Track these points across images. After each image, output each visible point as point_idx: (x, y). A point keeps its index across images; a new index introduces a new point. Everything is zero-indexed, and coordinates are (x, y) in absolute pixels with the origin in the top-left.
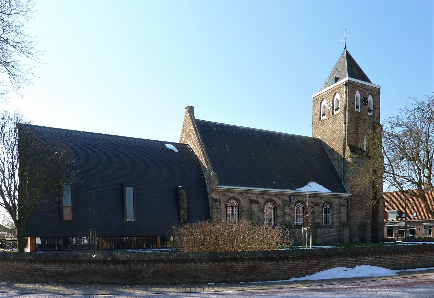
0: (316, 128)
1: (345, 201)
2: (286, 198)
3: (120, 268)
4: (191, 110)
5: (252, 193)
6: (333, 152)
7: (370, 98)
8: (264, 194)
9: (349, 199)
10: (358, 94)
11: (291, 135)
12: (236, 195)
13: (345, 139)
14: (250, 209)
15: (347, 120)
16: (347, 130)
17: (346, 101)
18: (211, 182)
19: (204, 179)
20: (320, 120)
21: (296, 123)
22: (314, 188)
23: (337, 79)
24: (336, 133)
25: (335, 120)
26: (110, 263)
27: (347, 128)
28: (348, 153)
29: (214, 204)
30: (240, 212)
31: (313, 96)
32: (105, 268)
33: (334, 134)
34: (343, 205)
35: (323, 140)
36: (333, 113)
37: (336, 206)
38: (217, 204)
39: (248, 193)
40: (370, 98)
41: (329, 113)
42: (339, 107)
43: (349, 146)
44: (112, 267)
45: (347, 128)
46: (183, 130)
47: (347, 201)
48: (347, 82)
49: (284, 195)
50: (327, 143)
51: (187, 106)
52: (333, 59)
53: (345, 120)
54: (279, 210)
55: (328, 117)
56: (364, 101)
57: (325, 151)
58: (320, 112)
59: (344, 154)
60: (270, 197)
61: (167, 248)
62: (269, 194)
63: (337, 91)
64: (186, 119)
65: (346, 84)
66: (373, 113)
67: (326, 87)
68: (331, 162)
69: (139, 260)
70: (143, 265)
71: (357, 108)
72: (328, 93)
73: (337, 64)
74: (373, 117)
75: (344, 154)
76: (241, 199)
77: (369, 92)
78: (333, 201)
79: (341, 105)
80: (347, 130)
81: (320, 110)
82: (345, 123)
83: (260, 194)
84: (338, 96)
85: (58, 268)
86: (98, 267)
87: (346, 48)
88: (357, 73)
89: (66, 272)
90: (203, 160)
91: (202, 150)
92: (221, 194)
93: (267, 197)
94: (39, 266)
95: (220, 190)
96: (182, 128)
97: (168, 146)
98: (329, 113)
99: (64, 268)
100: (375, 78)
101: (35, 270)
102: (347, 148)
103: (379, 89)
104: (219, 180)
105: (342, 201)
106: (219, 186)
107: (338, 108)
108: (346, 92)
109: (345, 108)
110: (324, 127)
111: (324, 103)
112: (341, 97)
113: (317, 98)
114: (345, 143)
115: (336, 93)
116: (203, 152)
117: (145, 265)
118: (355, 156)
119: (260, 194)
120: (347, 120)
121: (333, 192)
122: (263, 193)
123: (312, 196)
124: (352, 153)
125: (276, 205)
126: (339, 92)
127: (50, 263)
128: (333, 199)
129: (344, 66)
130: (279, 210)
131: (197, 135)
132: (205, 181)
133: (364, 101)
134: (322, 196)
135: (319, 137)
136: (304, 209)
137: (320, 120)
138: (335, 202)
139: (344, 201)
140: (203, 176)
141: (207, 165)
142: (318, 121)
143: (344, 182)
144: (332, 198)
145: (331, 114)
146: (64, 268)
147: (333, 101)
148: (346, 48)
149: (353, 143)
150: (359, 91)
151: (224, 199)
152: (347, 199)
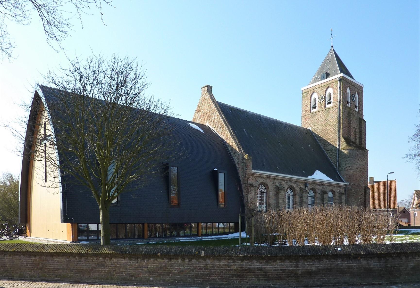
0: (305, 119)
1: (344, 190)
2: (303, 186)
3: (373, 264)
4: (209, 89)
5: (278, 179)
6: (325, 143)
7: (357, 95)
8: (287, 180)
9: (347, 189)
10: (348, 90)
11: (289, 124)
12: (265, 181)
13: (339, 131)
14: (277, 195)
15: (341, 113)
16: (341, 123)
17: (340, 95)
18: (245, 166)
19: (234, 163)
20: (310, 112)
21: (287, 111)
22: (319, 176)
23: (328, 75)
24: (329, 125)
25: (328, 113)
26: (361, 258)
27: (341, 121)
28: (343, 144)
29: (250, 189)
30: (267, 198)
31: (302, 89)
32: (354, 264)
33: (327, 126)
34: (343, 194)
35: (314, 131)
36: (325, 106)
37: (337, 194)
38: (252, 189)
39: (274, 179)
40: (357, 95)
41: (321, 106)
42: (332, 100)
43: (344, 138)
44: (363, 262)
45: (341, 121)
46: (198, 110)
47: (345, 190)
48: (341, 78)
49: (301, 182)
50: (319, 134)
51: (206, 85)
52: (319, 57)
53: (340, 113)
54: (298, 197)
55: (320, 110)
56: (353, 97)
57: (317, 142)
58: (311, 105)
59: (339, 146)
60: (291, 184)
61: (185, 236)
62: (291, 181)
63: (330, 85)
64: (204, 98)
65: (340, 80)
66: (359, 109)
67: (315, 81)
68: (324, 152)
69: (400, 253)
70: (401, 259)
71: (348, 103)
72: (320, 87)
73: (325, 62)
74: (359, 112)
75: (339, 146)
76: (269, 185)
77: (356, 89)
78: (335, 189)
79: (334, 100)
80: (341, 123)
81: (311, 102)
82: (339, 116)
83: (284, 181)
84: (330, 91)
85: (287, 267)
86: (345, 264)
87: (332, 47)
88: (344, 70)
89: (299, 272)
90: (231, 142)
91: (230, 132)
92: (254, 179)
93: (289, 184)
94: (256, 264)
95: (253, 175)
96: (196, 108)
97: (192, 125)
98: (321, 106)
99: (297, 266)
100: (358, 78)
101: (250, 271)
102: (342, 140)
103: (362, 88)
104: (253, 164)
105: (341, 190)
106: (253, 171)
107: (331, 102)
108: (340, 88)
109: (340, 102)
110: (315, 119)
111: (315, 96)
112: (334, 91)
113: (307, 91)
114: (339, 135)
115: (328, 87)
116: (231, 134)
117: (404, 258)
118: (351, 148)
119: (284, 181)
120: (341, 113)
121: (335, 181)
122: (286, 180)
123: (319, 183)
124: (348, 145)
125: (295, 192)
126: (332, 87)
127: (275, 261)
128: (336, 188)
129: (334, 63)
130: (298, 197)
131: (221, 116)
132: (235, 165)
133: (353, 97)
134: (329, 185)
135: (310, 128)
136: (315, 196)
137: (310, 112)
138: (337, 190)
139: (343, 190)
140: (233, 159)
141: (238, 148)
142: (308, 113)
143: (340, 172)
144: (335, 187)
145: (323, 107)
146: (297, 266)
147: (325, 95)
148: (332, 47)
149: (346, 136)
150: (350, 88)
151: (256, 184)
152: (345, 188)
